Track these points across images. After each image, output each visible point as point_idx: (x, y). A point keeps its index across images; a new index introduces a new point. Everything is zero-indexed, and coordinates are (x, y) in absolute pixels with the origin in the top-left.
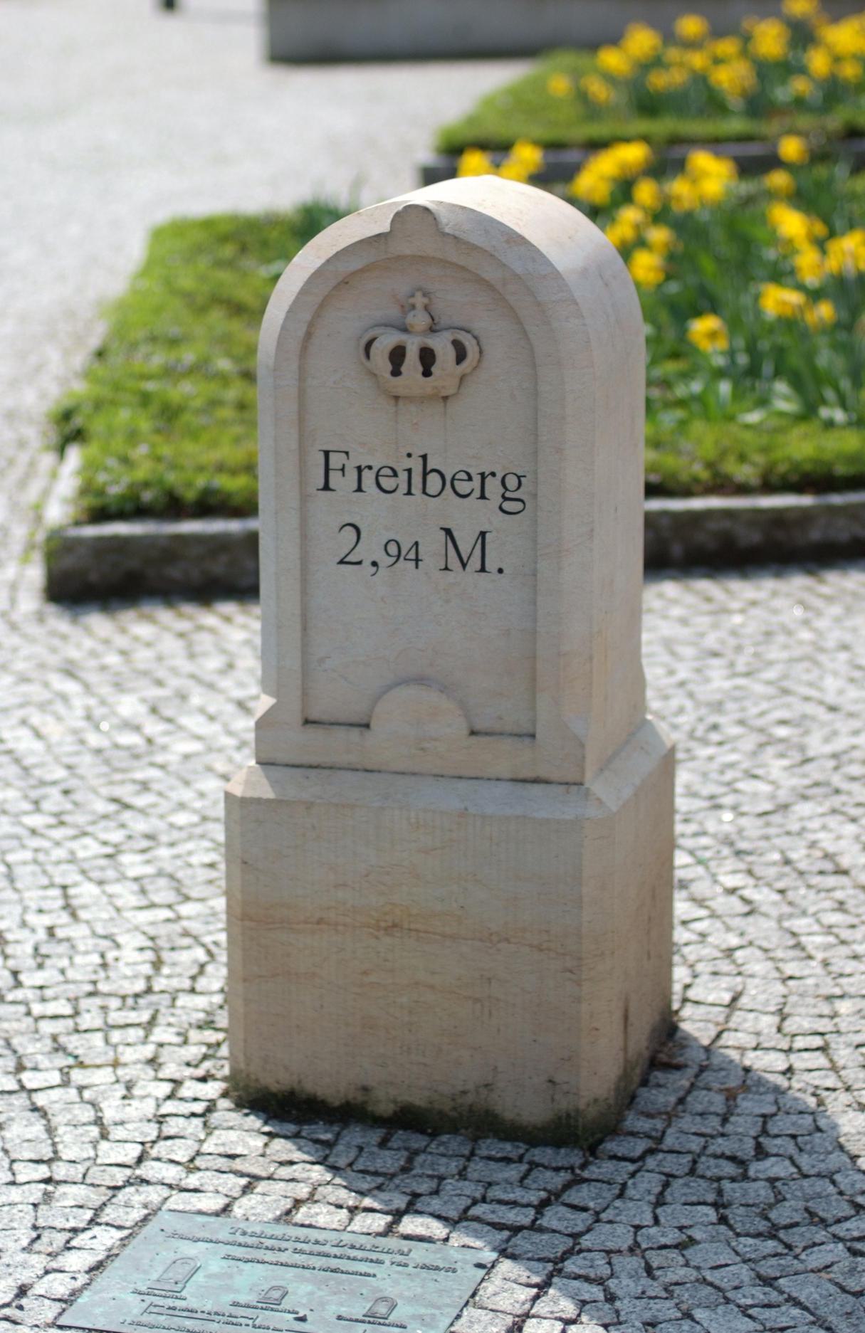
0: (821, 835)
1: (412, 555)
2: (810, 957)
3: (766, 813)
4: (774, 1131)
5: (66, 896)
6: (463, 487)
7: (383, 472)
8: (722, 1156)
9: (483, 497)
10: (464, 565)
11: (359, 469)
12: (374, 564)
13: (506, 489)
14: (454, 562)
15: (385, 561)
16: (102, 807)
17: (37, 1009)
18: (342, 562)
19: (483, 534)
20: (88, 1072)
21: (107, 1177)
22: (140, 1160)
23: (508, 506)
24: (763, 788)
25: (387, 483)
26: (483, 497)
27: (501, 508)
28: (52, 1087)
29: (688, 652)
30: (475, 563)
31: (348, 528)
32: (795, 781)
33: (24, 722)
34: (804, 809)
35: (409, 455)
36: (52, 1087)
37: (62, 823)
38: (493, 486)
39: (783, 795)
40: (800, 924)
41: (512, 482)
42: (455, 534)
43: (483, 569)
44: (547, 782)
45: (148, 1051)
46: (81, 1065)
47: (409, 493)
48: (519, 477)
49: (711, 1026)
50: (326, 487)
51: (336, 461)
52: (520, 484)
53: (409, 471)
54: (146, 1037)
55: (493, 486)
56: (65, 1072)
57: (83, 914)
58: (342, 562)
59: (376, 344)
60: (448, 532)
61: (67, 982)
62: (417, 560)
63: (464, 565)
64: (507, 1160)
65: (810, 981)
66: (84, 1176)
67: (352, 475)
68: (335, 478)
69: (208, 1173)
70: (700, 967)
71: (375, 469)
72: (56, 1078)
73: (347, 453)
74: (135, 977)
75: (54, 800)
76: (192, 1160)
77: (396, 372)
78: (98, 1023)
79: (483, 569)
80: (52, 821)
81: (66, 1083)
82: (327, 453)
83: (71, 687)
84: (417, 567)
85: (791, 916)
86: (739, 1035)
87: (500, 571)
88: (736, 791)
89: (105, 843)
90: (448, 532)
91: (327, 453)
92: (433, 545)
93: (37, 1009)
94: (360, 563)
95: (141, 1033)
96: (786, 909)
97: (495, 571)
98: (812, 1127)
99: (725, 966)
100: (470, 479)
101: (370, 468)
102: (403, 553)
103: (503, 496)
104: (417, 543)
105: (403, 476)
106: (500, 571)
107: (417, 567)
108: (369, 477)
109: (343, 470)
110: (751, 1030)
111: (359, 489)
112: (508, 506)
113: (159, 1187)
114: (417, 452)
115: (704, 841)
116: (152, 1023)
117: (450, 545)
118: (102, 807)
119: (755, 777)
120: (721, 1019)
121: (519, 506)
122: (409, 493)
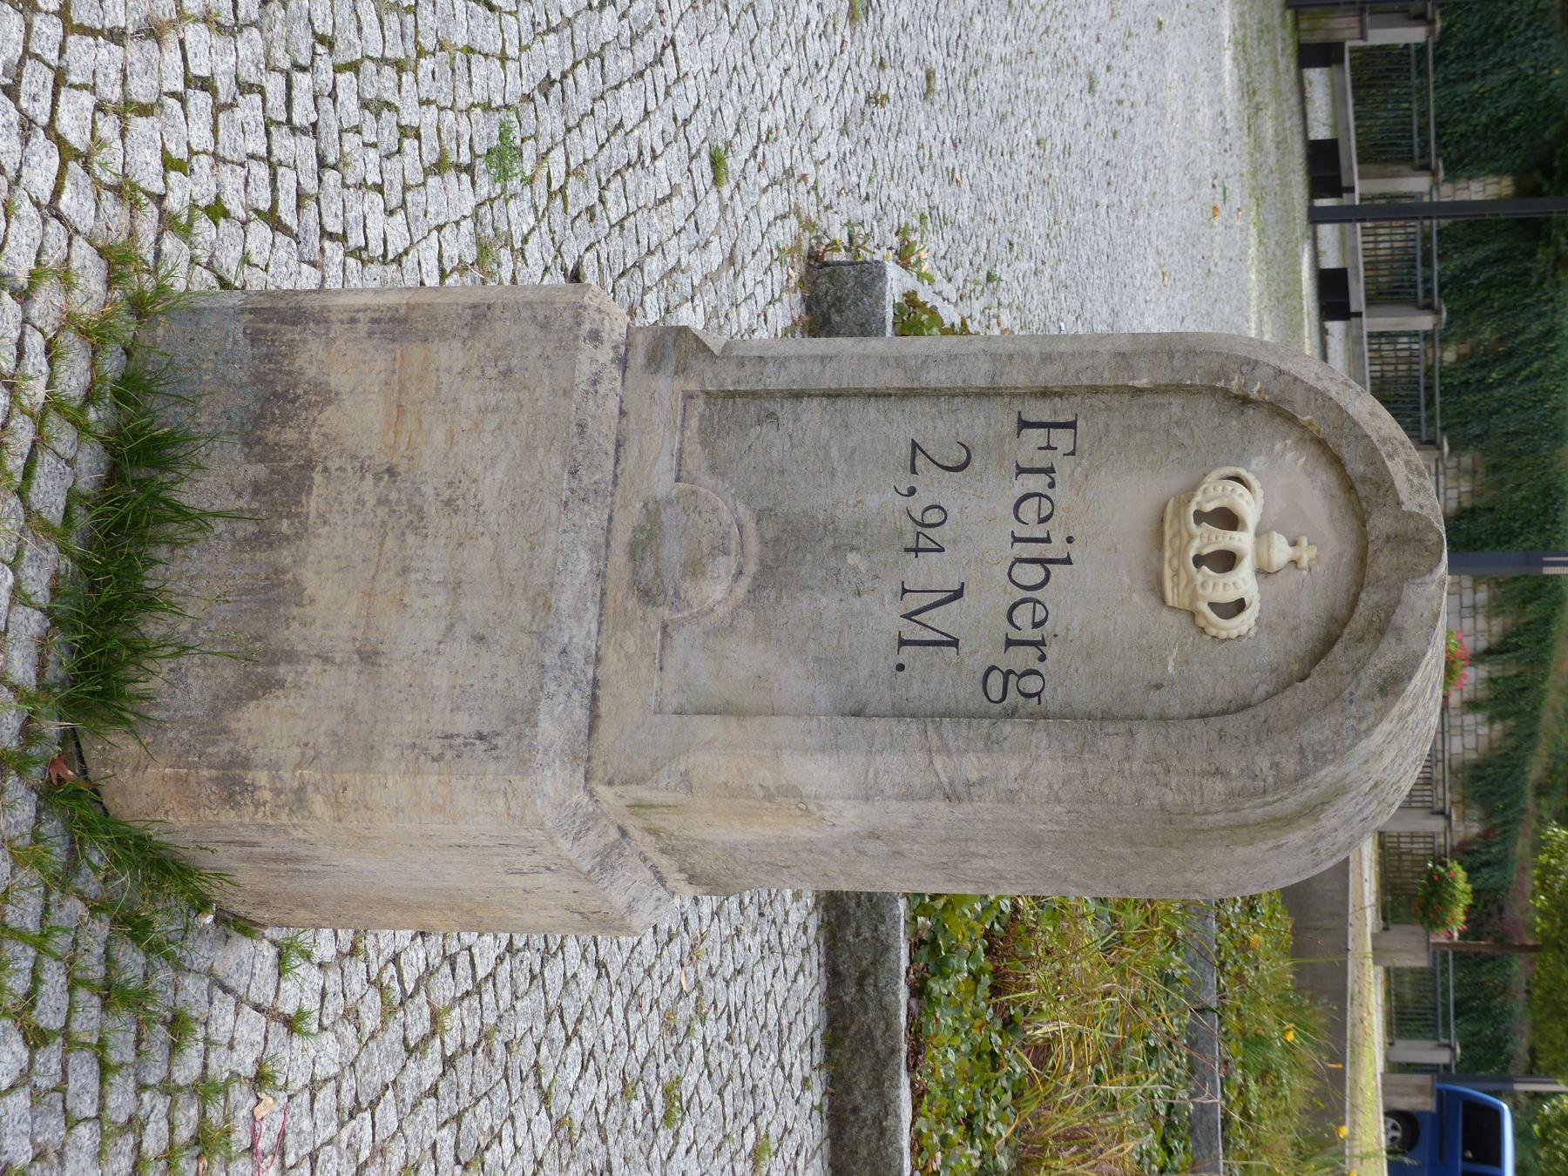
0: (508, 1145)
1: (923, 543)
2: (341, 1125)
3: (538, 1076)
4: (74, 1060)
5: (459, 168)
6: (1023, 616)
7: (1046, 504)
8: (36, 979)
9: (1010, 643)
10: (908, 616)
11: (1049, 471)
12: (912, 491)
13: (1021, 676)
14: (914, 602)
15: (916, 505)
16: (572, 251)
17: (302, 81)
18: (915, 445)
19: (954, 643)
20: (207, 117)
21: (34, 90)
22: (60, 141)
23: (996, 680)
24: (572, 1073)
25: (1029, 509)
26: (1010, 643)
27: (993, 668)
28: (185, 59)
29: (735, 994)
30: (914, 632)
31: (964, 458)
32: (578, 1117)
33: (675, 189)
34: (543, 1127)
35: (1070, 540)
36: (185, 59)
37: (551, 196)
38: (1023, 658)
39: (561, 1100)
40: (388, 1114)
41: (1032, 684)
42: (955, 603)
43: (903, 643)
44: (592, 729)
45: (234, 205)
46: (218, 108)
47: (1016, 540)
48: (1038, 694)
49: (245, 979)
50: (1024, 425)
51: (1062, 438)
52: (1028, 696)
53: (1047, 540)
54: (257, 211)
55: (1023, 658)
56: (206, 84)
57: (433, 181)
58: (915, 445)
59: (1240, 488)
60: (958, 594)
61: (341, 131)
62: (917, 550)
63: (908, 616)
64: (41, 667)
65: (306, 1125)
66: (37, 57)
67: (1042, 460)
68: (1036, 436)
69: (38, 234)
70: (334, 976)
71: (1049, 492)
72: (200, 68)
73: (1073, 453)
74: (345, 223)
75: (582, 196)
76: (59, 217)
77: (1200, 517)
78: (278, 153)
79: (903, 643)
80: (559, 201)
81: (189, 80)
82: (1071, 425)
83: (715, 257)
84: (907, 550)
85: (400, 1101)
86: (230, 1018)
87: (901, 667)
88: (568, 1040)
89: (525, 240)
90: (958, 594)
91: (1071, 425)
92: (932, 572)
93: (302, 81)
94: (914, 471)
95: (264, 206)
96: (409, 1097)
97: (902, 659)
98: (77, 1114)
99: (335, 1006)
100: (1042, 521)
101: (1052, 485)
102: (927, 531)
103: (1010, 672)
104: (941, 550)
105: (1040, 532)
106: (901, 667)
107: (907, 550)
108: (1037, 483)
109: (1049, 447)
110: (237, 1035)
111: (1021, 471)
112: (996, 680)
113: (17, 157)
114: (1075, 552)
115: (506, 995)
116: (277, 225)
117: (939, 596)
118: (572, 251)
119: (584, 1068)
120: (254, 996)
121: (996, 693)
122: (1016, 540)
